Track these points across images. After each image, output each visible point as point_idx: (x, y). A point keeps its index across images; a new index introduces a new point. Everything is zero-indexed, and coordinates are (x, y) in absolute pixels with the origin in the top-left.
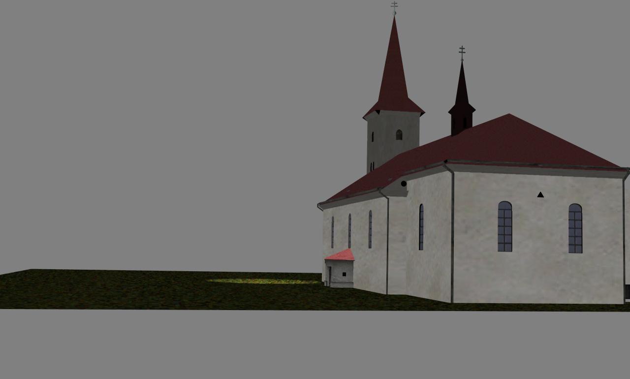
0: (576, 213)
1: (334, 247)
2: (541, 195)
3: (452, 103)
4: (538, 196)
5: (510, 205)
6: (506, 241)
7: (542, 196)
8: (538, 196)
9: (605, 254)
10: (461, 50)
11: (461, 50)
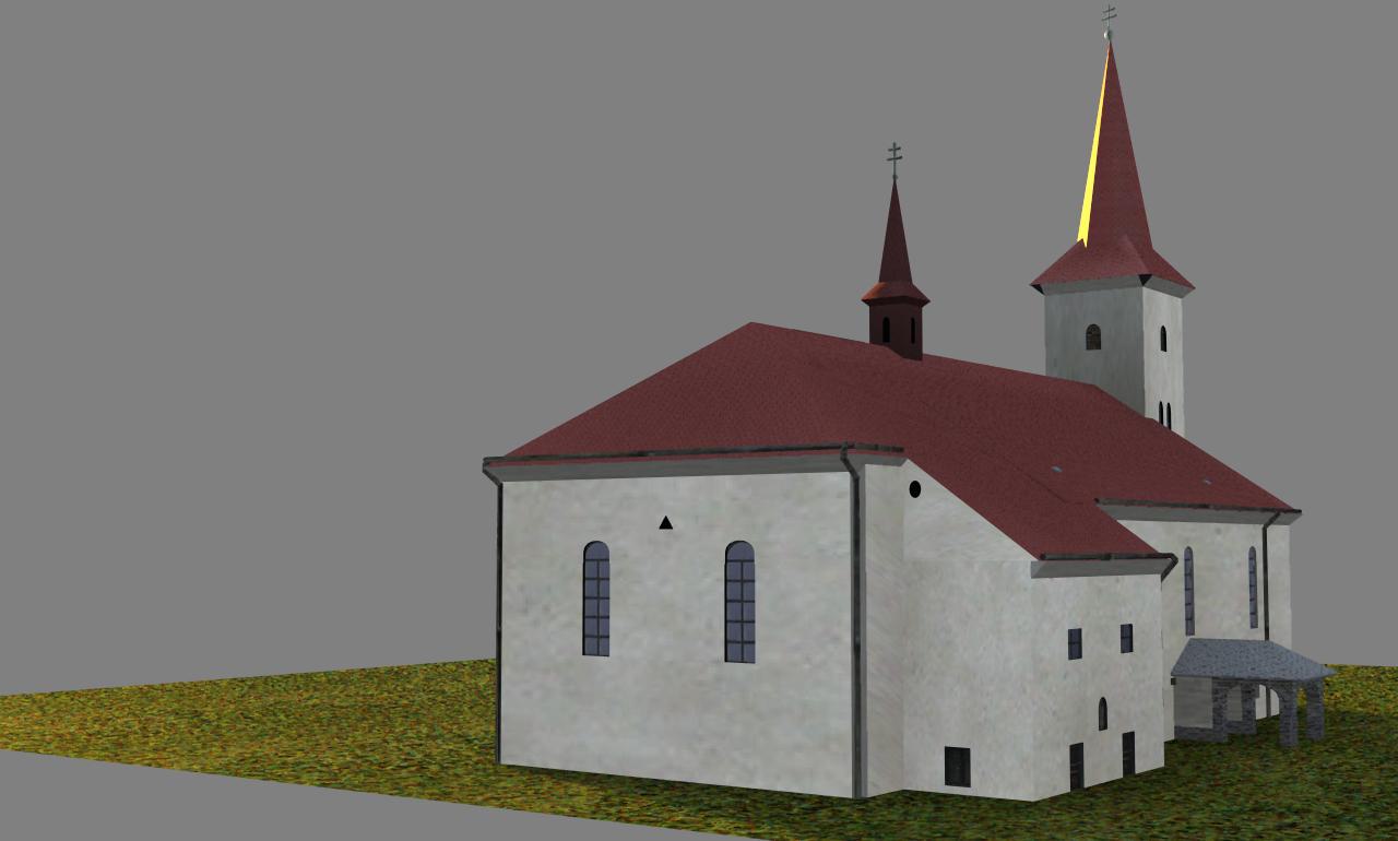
0: (739, 564)
1: (1064, 756)
2: (666, 524)
3: (870, 280)
4: (670, 527)
5: (592, 547)
6: (601, 634)
7: (666, 520)
8: (670, 527)
9: (807, 666)
10: (891, 155)
11: (891, 155)
